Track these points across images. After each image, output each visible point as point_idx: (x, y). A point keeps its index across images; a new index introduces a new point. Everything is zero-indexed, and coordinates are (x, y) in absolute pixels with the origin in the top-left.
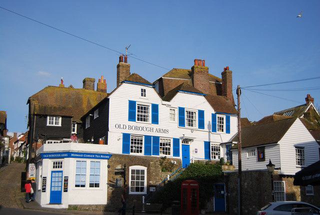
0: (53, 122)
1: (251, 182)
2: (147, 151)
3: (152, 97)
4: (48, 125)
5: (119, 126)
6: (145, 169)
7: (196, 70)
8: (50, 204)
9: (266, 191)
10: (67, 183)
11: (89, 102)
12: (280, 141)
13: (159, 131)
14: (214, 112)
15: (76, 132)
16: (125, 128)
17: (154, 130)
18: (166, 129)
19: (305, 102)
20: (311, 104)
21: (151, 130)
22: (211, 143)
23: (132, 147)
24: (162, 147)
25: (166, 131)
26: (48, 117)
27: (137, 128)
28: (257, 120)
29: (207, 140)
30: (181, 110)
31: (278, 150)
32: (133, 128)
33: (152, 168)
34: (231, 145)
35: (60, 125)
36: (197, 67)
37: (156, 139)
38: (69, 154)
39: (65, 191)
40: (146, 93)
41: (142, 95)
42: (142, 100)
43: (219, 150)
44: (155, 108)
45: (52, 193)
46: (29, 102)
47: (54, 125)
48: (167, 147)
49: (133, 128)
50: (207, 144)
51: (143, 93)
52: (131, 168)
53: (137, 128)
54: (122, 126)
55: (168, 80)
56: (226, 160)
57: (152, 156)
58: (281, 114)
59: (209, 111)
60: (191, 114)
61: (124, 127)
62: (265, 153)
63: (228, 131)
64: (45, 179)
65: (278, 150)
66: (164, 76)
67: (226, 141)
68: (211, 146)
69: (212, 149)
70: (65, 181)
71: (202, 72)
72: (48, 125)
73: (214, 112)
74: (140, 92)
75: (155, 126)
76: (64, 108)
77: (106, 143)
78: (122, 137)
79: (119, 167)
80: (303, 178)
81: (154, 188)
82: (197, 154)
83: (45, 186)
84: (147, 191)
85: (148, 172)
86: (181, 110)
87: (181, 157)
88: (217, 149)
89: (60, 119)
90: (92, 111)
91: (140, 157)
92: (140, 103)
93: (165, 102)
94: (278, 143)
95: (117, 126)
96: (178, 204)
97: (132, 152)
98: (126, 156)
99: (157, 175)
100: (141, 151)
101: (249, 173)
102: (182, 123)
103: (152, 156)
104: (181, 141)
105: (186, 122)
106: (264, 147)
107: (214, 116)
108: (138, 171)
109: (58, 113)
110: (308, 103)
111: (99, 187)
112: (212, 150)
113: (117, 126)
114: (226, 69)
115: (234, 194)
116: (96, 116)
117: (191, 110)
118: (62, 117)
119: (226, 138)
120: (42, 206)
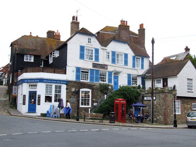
0: (28, 59)
1: (159, 101)
2: (92, 79)
3: (95, 43)
4: (25, 60)
6: (90, 90)
8: (28, 112)
9: (169, 107)
10: (40, 99)
14: (134, 55)
15: (42, 66)
23: (84, 74)
24: (101, 79)
28: (33, 36)
29: (75, 15)
30: (114, 53)
38: (41, 80)
39: (38, 105)
41: (89, 42)
42: (88, 46)
44: (97, 51)
46: (12, 45)
47: (29, 61)
52: (81, 90)
56: (141, 86)
58: (177, 56)
59: (131, 54)
62: (168, 82)
64: (24, 96)
66: (101, 31)
69: (132, 79)
70: (38, 97)
72: (25, 60)
76: (35, 50)
79: (73, 90)
81: (97, 103)
82: (123, 82)
83: (25, 101)
84: (91, 105)
86: (114, 53)
87: (113, 84)
93: (102, 47)
94: (177, 76)
96: (114, 114)
97: (82, 79)
103: (94, 82)
104: (113, 73)
105: (110, 54)
107: (134, 57)
109: (31, 53)
112: (132, 79)
115: (147, 108)
119: (141, 72)
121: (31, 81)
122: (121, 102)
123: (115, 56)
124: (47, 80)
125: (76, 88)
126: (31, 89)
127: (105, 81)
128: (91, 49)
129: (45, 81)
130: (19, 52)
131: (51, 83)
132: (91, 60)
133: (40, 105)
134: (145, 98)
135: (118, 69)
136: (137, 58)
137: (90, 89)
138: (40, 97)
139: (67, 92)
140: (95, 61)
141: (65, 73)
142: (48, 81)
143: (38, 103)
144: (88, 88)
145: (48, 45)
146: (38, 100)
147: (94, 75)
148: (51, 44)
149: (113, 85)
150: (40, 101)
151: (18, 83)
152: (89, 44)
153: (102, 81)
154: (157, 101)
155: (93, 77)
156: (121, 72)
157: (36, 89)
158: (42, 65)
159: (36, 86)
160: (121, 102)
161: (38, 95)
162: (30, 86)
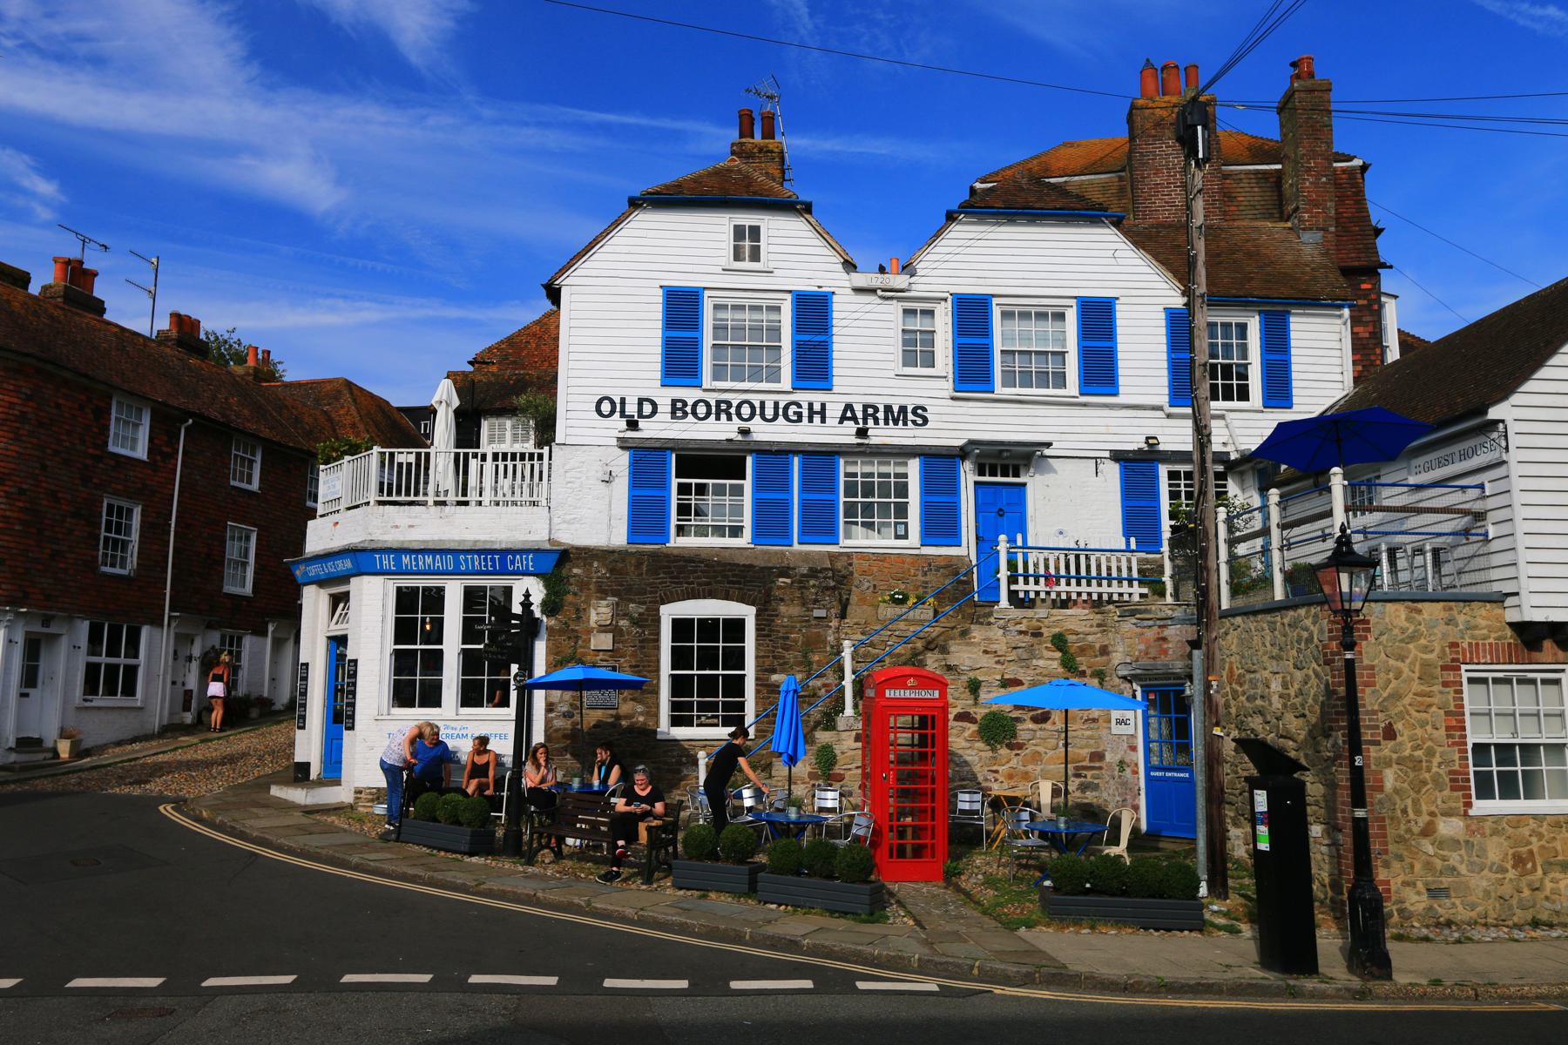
6: (747, 613)
40: (763, 244)
41: (738, 256)
51: (747, 244)
52: (670, 612)
73: (1178, 301)
85: (759, 629)
92: (730, 299)
95: (606, 407)
97: (1215, 397)
101: (1305, 810)
105: (943, 324)
107: (1180, 327)
108: (708, 627)
113: (606, 407)
114: (855, 267)
120: (545, 592)
122: (889, 693)
128: (764, 300)
137: (742, 599)
140: (1081, 394)
147: (787, 488)
151: (1351, 513)
155: (786, 505)
160: (889, 693)
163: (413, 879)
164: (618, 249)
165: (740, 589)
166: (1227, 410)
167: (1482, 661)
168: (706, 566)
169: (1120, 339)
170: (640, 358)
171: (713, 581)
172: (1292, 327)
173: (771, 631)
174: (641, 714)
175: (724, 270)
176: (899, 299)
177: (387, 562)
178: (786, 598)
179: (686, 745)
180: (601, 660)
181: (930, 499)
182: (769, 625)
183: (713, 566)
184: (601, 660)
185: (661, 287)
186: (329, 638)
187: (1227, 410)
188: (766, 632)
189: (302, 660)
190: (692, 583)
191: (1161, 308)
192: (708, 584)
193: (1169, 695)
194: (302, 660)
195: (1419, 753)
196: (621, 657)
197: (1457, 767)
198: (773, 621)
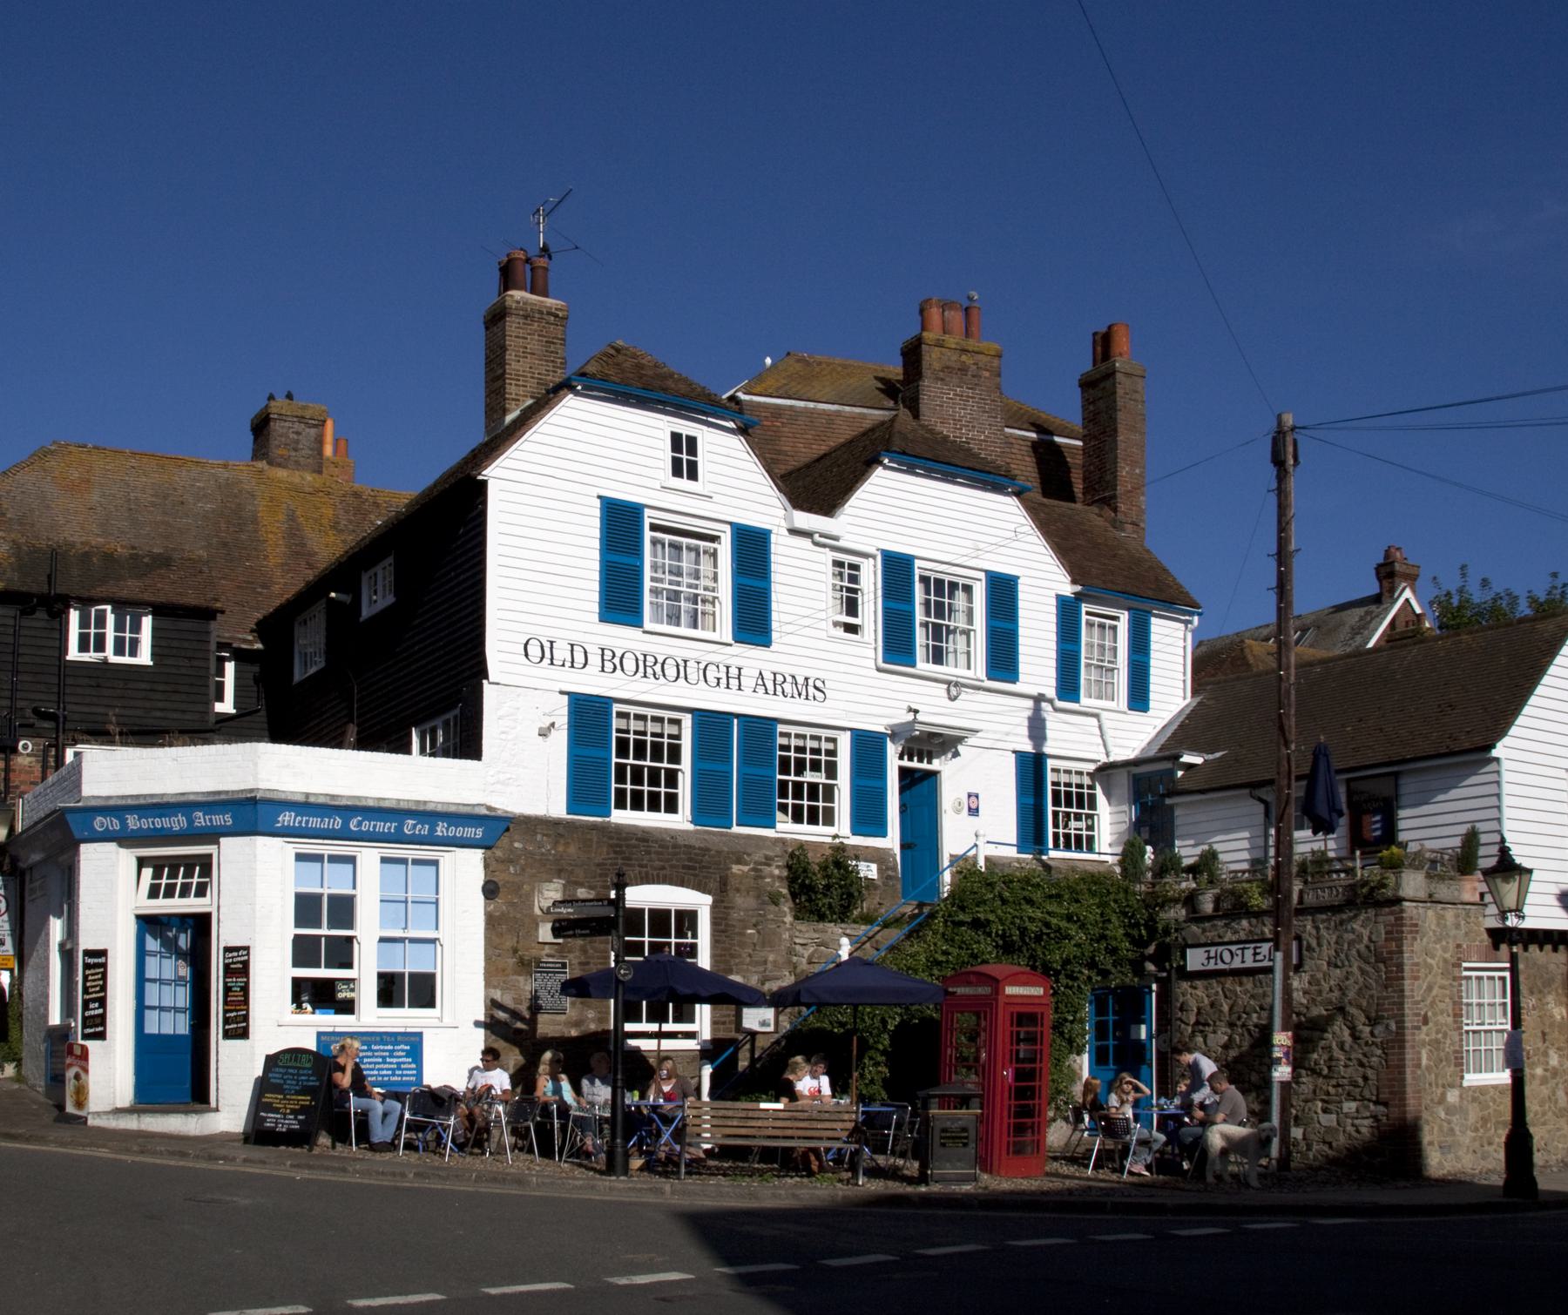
2: (709, 804)
5: (547, 653)
6: (700, 902)
7: (932, 358)
10: (245, 989)
11: (294, 533)
12: (1506, 741)
13: (775, 684)
16: (579, 658)
17: (748, 682)
18: (812, 674)
19: (1373, 588)
20: (1408, 594)
21: (732, 678)
22: (1050, 763)
25: (810, 688)
26: (74, 616)
27: (647, 666)
30: (897, 569)
31: (1492, 789)
32: (629, 664)
33: (743, 903)
34: (1172, 772)
35: (144, 657)
36: (940, 344)
37: (760, 729)
39: (228, 1035)
41: (677, 472)
43: (1093, 805)
45: (147, 1047)
48: (809, 777)
49: (629, 664)
50: (1032, 768)
53: (647, 666)
54: (562, 653)
55: (777, 412)
57: (736, 829)
60: (942, 588)
61: (577, 657)
63: (1139, 697)
65: (1492, 789)
67: (1130, 754)
68: (1050, 777)
69: (1056, 794)
70: (228, 971)
71: (963, 370)
72: (73, 654)
73: (1068, 589)
74: (668, 454)
75: (750, 658)
77: (466, 744)
78: (562, 720)
80: (732, 1049)
83: (102, 1002)
85: (715, 922)
87: (891, 841)
88: (1080, 796)
89: (147, 622)
90: (347, 571)
91: (673, 834)
93: (804, 520)
95: (534, 650)
97: (621, 805)
98: (594, 827)
99: (767, 941)
100: (672, 806)
102: (898, 647)
103: (736, 829)
104: (892, 750)
105: (871, 580)
106: (1396, 775)
107: (1067, 612)
109: (131, 588)
110: (1392, 590)
111: (430, 1003)
112: (1056, 802)
113: (534, 650)
116: (376, 598)
117: (948, 574)
118: (159, 611)
121: (159, 823)
123: (909, 599)
124: (306, 806)
125: (571, 884)
126: (154, 893)
127: (829, 819)
129: (287, 818)
130: (16, 576)
131: (344, 835)
132: (847, 559)
133: (244, 1034)
134: (1195, 959)
135: (936, 710)
136: (1088, 613)
137: (701, 887)
138: (246, 964)
139: (492, 922)
141: (766, 643)
142: (315, 822)
143: (226, 1021)
144: (681, 883)
145: (272, 528)
146: (227, 989)
148: (292, 517)
149: (897, 851)
150: (246, 1002)
152: (684, 483)
153: (797, 818)
154: (1313, 981)
156: (960, 740)
157: (201, 891)
158: (221, 698)
159: (206, 870)
161: (228, 950)
162: (148, 873)
163: (1474, 1063)
164: (547, 440)
165: (695, 875)
166: (1102, 709)
167: (152, 998)
168: (660, 846)
169: (1021, 622)
170: (574, 583)
171: (667, 865)
172: (1153, 629)
173: (727, 925)
174: (593, 1020)
175: (711, 497)
176: (834, 549)
177: (287, 818)
178: (743, 888)
179: (645, 1054)
180: (548, 956)
181: (707, 766)
182: (726, 919)
183: (668, 848)
184: (548, 956)
185: (599, 497)
186: (139, 918)
187: (1102, 709)
188: (723, 927)
189: (86, 941)
190: (646, 866)
191: (1053, 594)
192: (663, 868)
193: (228, 1030)
194: (86, 941)
195: (1440, 1036)
196: (569, 952)
197: (1457, 1048)
198: (728, 914)
